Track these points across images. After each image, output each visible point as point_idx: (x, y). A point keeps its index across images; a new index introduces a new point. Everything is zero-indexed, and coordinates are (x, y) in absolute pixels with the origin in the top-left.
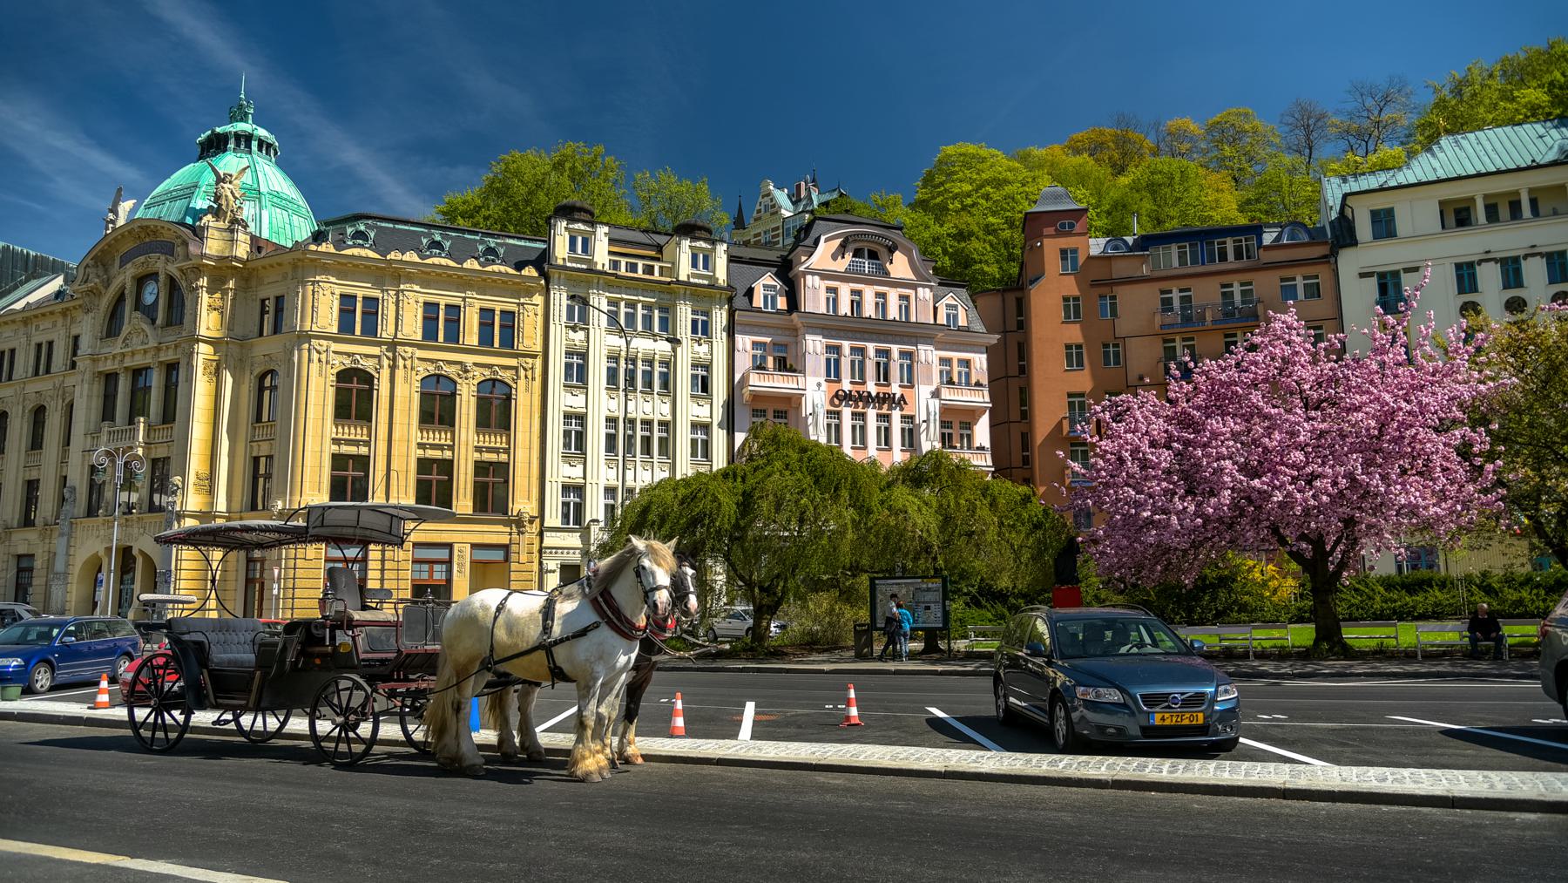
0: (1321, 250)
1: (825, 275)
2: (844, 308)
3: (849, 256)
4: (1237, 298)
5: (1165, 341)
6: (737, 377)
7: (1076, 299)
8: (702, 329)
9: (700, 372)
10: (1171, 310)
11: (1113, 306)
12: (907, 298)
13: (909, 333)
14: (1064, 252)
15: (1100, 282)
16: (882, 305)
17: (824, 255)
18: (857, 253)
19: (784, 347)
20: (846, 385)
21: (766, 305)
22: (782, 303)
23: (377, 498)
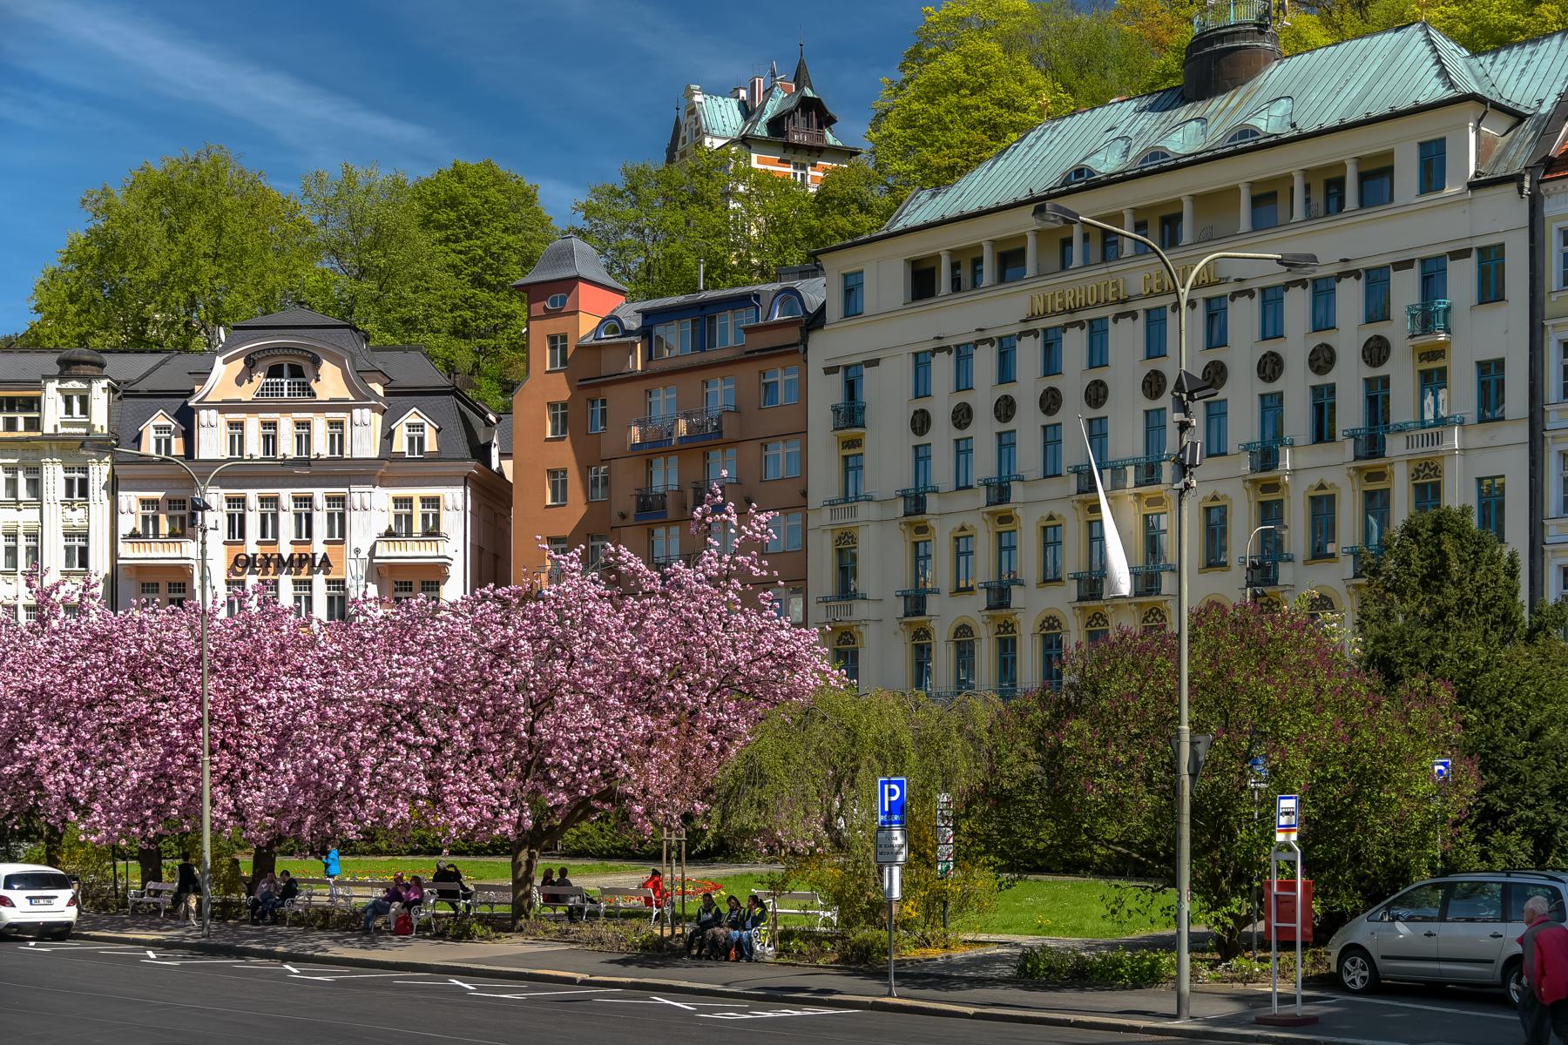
1: (224, 407)
2: (254, 447)
3: (259, 379)
7: (564, 406)
8: (78, 490)
9: (77, 543)
11: (604, 412)
12: (340, 424)
13: (344, 471)
14: (553, 339)
16: (304, 440)
17: (223, 379)
18: (275, 372)
20: (251, 547)
21: (158, 450)
22: (177, 447)
23: (1169, 629)
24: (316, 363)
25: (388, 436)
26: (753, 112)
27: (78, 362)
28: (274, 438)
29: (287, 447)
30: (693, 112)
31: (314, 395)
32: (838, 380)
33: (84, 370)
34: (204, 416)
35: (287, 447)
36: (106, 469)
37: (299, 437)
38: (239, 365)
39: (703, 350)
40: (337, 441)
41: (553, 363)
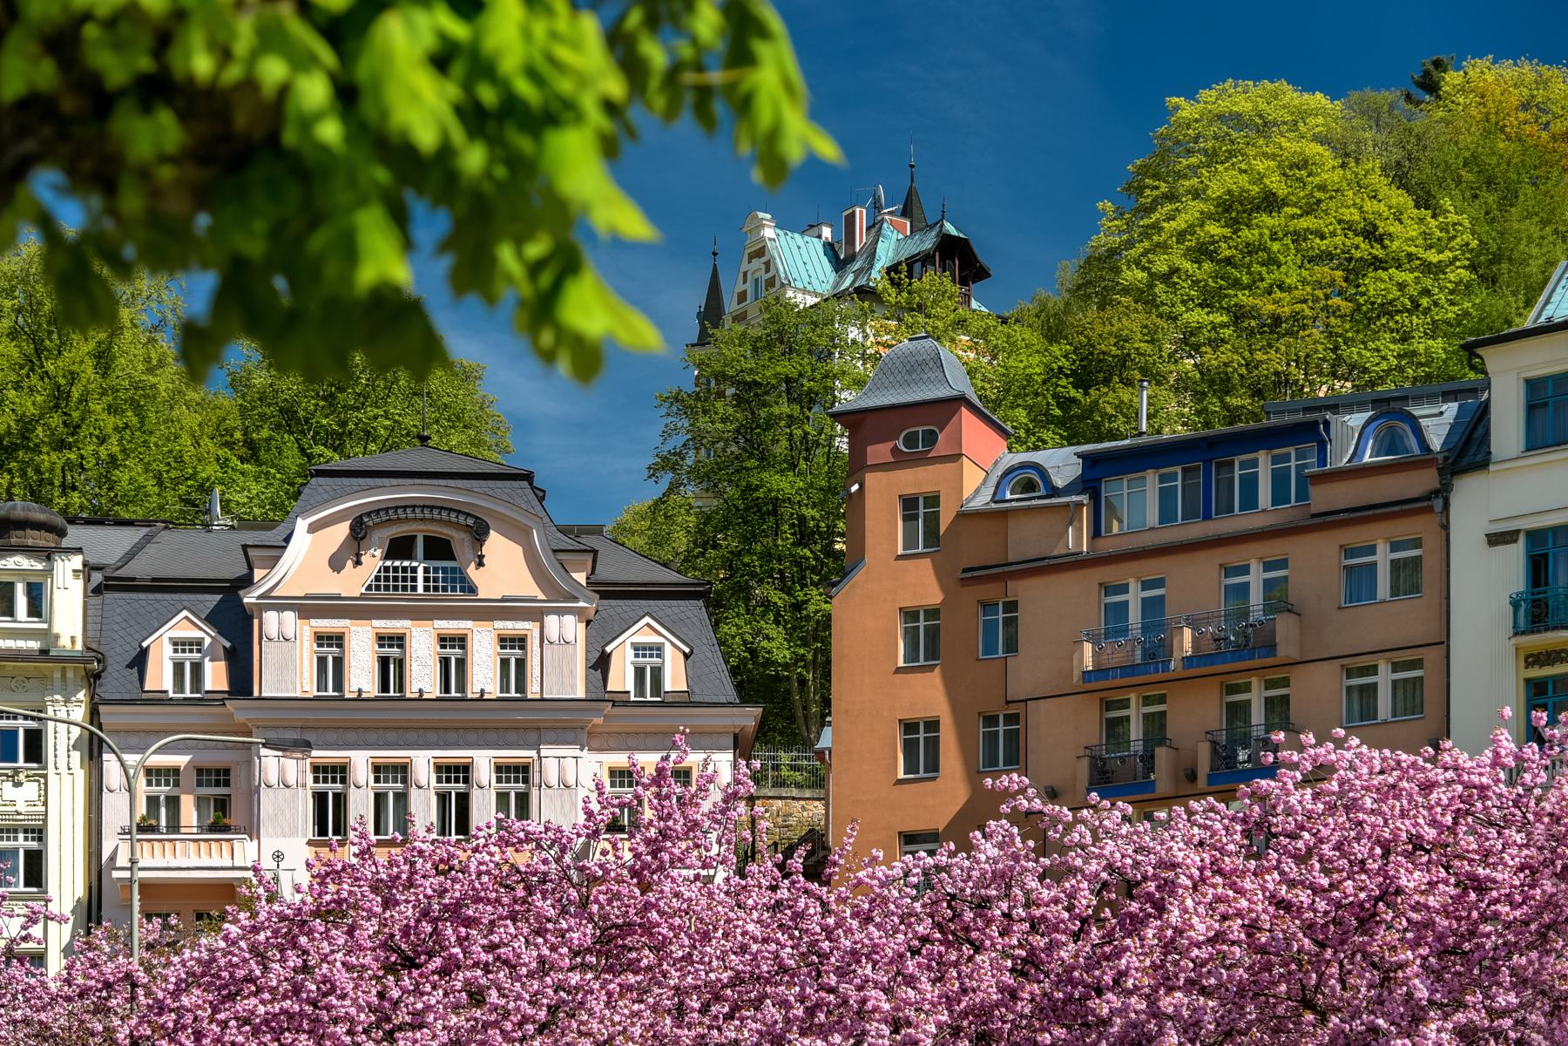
0: (1425, 480)
1: (308, 608)
2: (362, 677)
4: (1256, 597)
5: (1109, 705)
6: (105, 857)
7: (932, 613)
10: (1125, 631)
12: (520, 642)
13: (524, 720)
14: (909, 503)
15: (986, 570)
16: (453, 668)
17: (308, 556)
18: (399, 548)
19: (222, 776)
22: (215, 676)
24: (479, 533)
25: (601, 664)
26: (852, 258)
27: (24, 524)
28: (400, 663)
29: (423, 677)
30: (761, 252)
31: (472, 589)
32: (1516, 553)
33: (33, 538)
34: (271, 621)
35: (423, 677)
36: (79, 713)
37: (445, 662)
38: (342, 530)
39: (1207, 516)
40: (514, 669)
41: (910, 542)
